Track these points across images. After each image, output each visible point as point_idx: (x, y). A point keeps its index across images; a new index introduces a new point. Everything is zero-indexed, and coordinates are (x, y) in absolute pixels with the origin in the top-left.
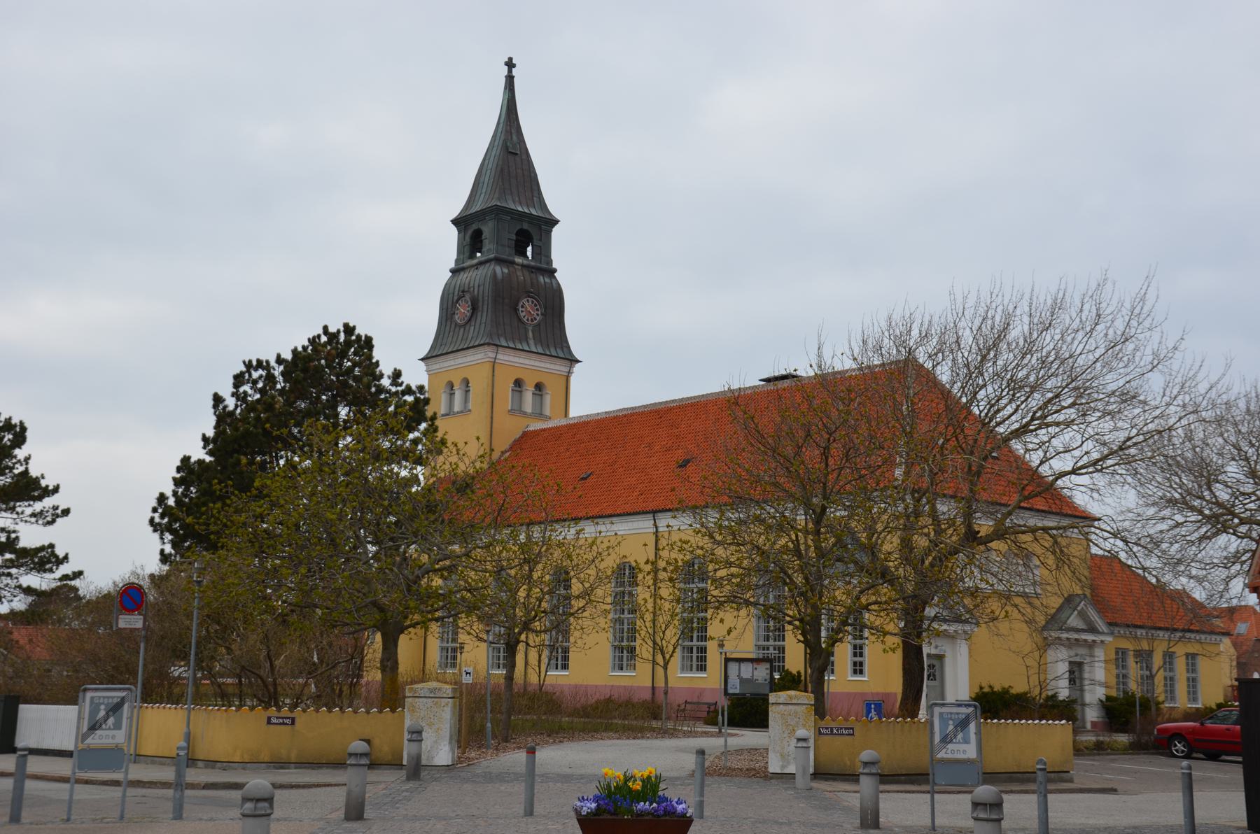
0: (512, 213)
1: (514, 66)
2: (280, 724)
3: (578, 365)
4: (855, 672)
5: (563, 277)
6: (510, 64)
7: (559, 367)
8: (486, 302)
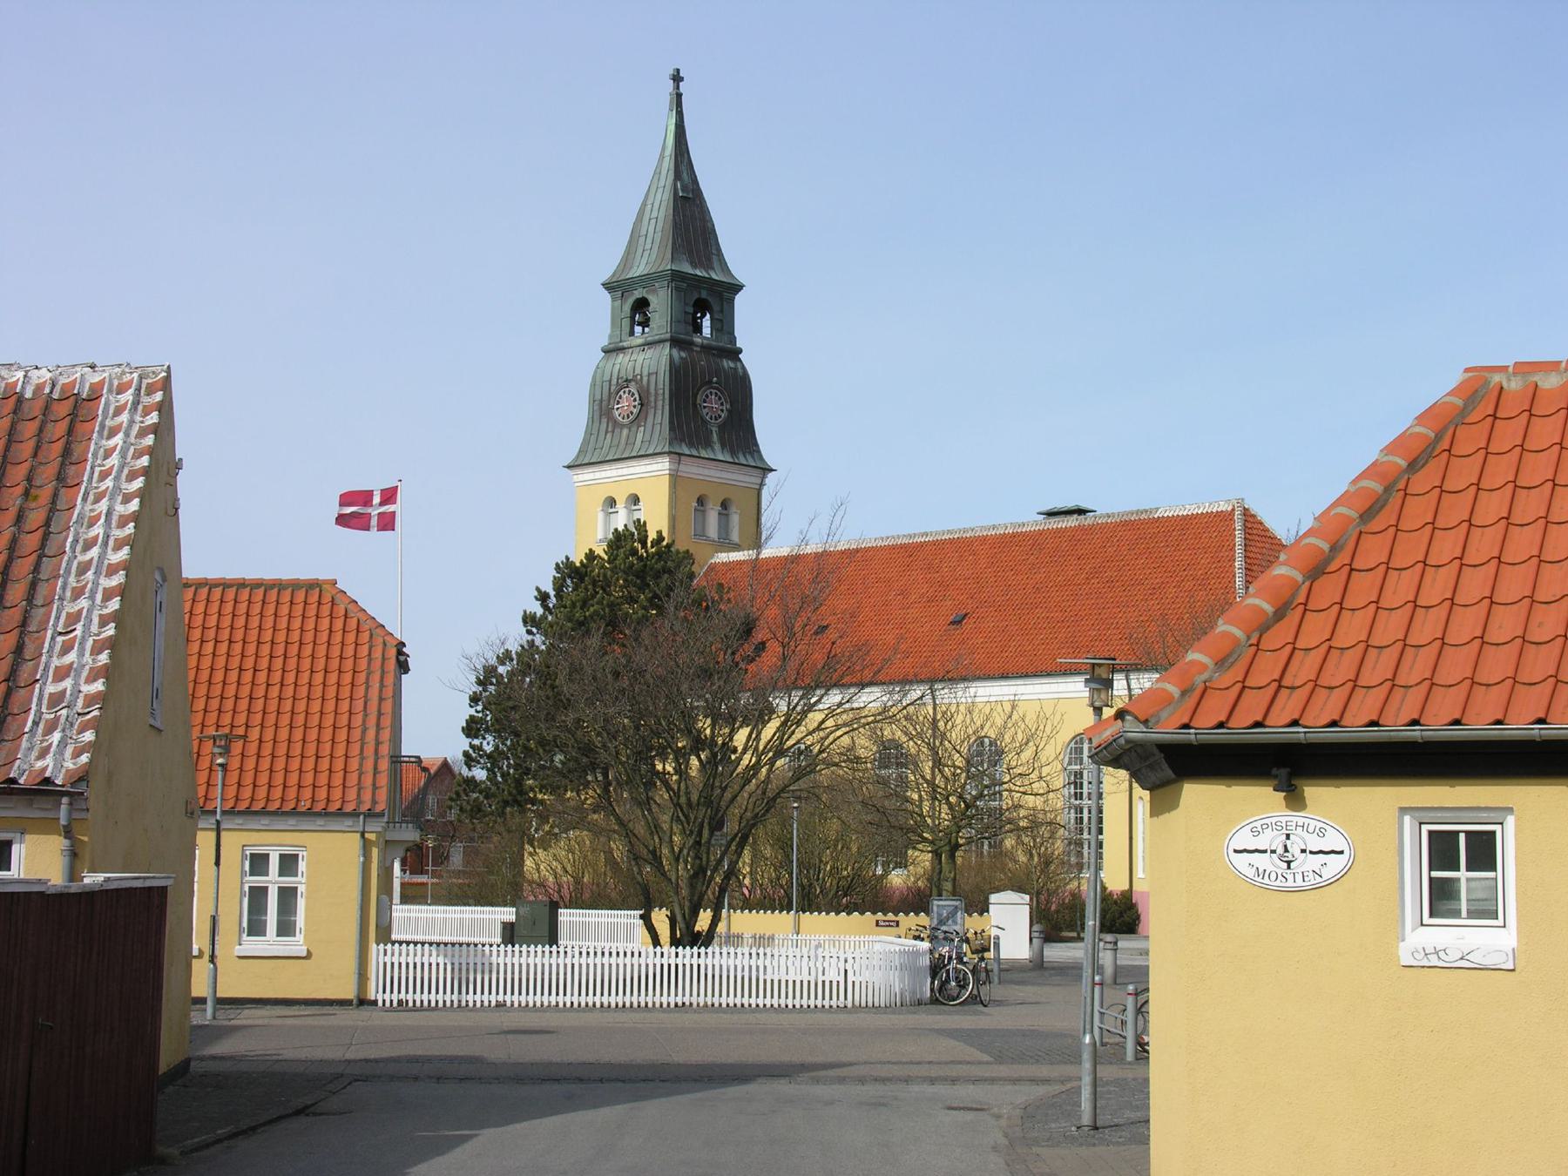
0: (689, 279)
1: (682, 79)
2: (887, 926)
3: (771, 475)
4: (1442, 898)
5: (750, 360)
6: (677, 78)
7: (751, 479)
8: (661, 397)
